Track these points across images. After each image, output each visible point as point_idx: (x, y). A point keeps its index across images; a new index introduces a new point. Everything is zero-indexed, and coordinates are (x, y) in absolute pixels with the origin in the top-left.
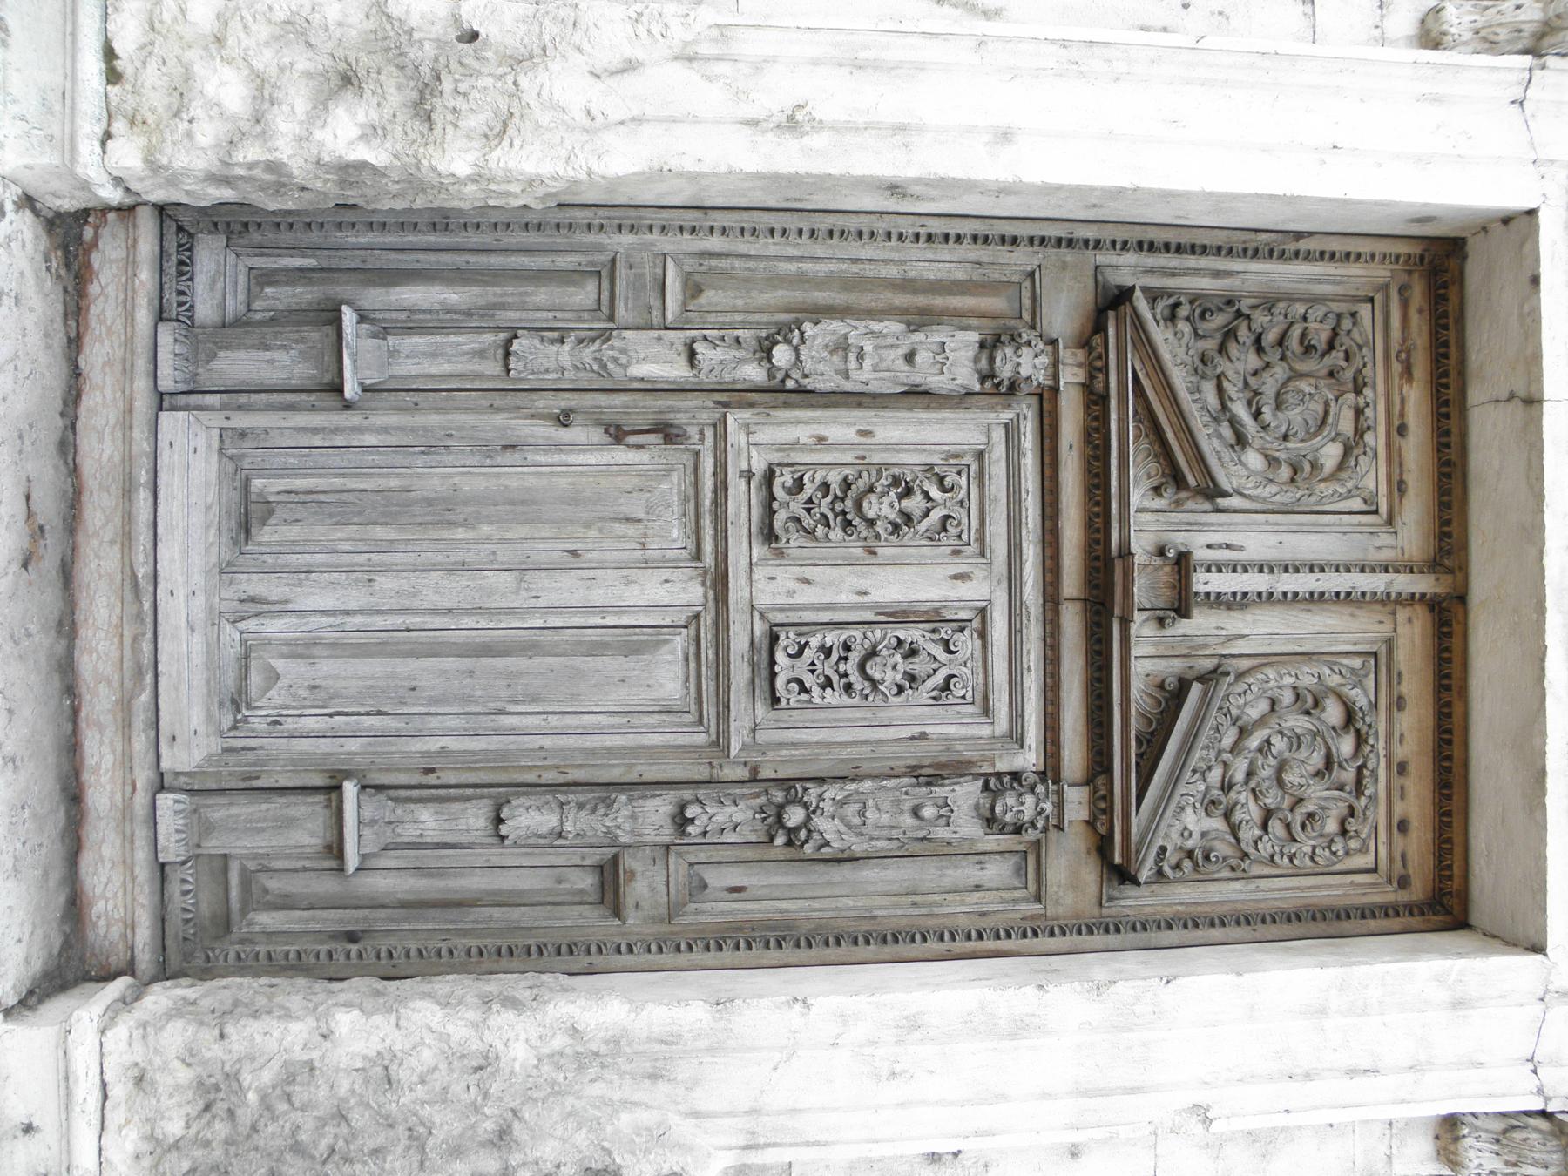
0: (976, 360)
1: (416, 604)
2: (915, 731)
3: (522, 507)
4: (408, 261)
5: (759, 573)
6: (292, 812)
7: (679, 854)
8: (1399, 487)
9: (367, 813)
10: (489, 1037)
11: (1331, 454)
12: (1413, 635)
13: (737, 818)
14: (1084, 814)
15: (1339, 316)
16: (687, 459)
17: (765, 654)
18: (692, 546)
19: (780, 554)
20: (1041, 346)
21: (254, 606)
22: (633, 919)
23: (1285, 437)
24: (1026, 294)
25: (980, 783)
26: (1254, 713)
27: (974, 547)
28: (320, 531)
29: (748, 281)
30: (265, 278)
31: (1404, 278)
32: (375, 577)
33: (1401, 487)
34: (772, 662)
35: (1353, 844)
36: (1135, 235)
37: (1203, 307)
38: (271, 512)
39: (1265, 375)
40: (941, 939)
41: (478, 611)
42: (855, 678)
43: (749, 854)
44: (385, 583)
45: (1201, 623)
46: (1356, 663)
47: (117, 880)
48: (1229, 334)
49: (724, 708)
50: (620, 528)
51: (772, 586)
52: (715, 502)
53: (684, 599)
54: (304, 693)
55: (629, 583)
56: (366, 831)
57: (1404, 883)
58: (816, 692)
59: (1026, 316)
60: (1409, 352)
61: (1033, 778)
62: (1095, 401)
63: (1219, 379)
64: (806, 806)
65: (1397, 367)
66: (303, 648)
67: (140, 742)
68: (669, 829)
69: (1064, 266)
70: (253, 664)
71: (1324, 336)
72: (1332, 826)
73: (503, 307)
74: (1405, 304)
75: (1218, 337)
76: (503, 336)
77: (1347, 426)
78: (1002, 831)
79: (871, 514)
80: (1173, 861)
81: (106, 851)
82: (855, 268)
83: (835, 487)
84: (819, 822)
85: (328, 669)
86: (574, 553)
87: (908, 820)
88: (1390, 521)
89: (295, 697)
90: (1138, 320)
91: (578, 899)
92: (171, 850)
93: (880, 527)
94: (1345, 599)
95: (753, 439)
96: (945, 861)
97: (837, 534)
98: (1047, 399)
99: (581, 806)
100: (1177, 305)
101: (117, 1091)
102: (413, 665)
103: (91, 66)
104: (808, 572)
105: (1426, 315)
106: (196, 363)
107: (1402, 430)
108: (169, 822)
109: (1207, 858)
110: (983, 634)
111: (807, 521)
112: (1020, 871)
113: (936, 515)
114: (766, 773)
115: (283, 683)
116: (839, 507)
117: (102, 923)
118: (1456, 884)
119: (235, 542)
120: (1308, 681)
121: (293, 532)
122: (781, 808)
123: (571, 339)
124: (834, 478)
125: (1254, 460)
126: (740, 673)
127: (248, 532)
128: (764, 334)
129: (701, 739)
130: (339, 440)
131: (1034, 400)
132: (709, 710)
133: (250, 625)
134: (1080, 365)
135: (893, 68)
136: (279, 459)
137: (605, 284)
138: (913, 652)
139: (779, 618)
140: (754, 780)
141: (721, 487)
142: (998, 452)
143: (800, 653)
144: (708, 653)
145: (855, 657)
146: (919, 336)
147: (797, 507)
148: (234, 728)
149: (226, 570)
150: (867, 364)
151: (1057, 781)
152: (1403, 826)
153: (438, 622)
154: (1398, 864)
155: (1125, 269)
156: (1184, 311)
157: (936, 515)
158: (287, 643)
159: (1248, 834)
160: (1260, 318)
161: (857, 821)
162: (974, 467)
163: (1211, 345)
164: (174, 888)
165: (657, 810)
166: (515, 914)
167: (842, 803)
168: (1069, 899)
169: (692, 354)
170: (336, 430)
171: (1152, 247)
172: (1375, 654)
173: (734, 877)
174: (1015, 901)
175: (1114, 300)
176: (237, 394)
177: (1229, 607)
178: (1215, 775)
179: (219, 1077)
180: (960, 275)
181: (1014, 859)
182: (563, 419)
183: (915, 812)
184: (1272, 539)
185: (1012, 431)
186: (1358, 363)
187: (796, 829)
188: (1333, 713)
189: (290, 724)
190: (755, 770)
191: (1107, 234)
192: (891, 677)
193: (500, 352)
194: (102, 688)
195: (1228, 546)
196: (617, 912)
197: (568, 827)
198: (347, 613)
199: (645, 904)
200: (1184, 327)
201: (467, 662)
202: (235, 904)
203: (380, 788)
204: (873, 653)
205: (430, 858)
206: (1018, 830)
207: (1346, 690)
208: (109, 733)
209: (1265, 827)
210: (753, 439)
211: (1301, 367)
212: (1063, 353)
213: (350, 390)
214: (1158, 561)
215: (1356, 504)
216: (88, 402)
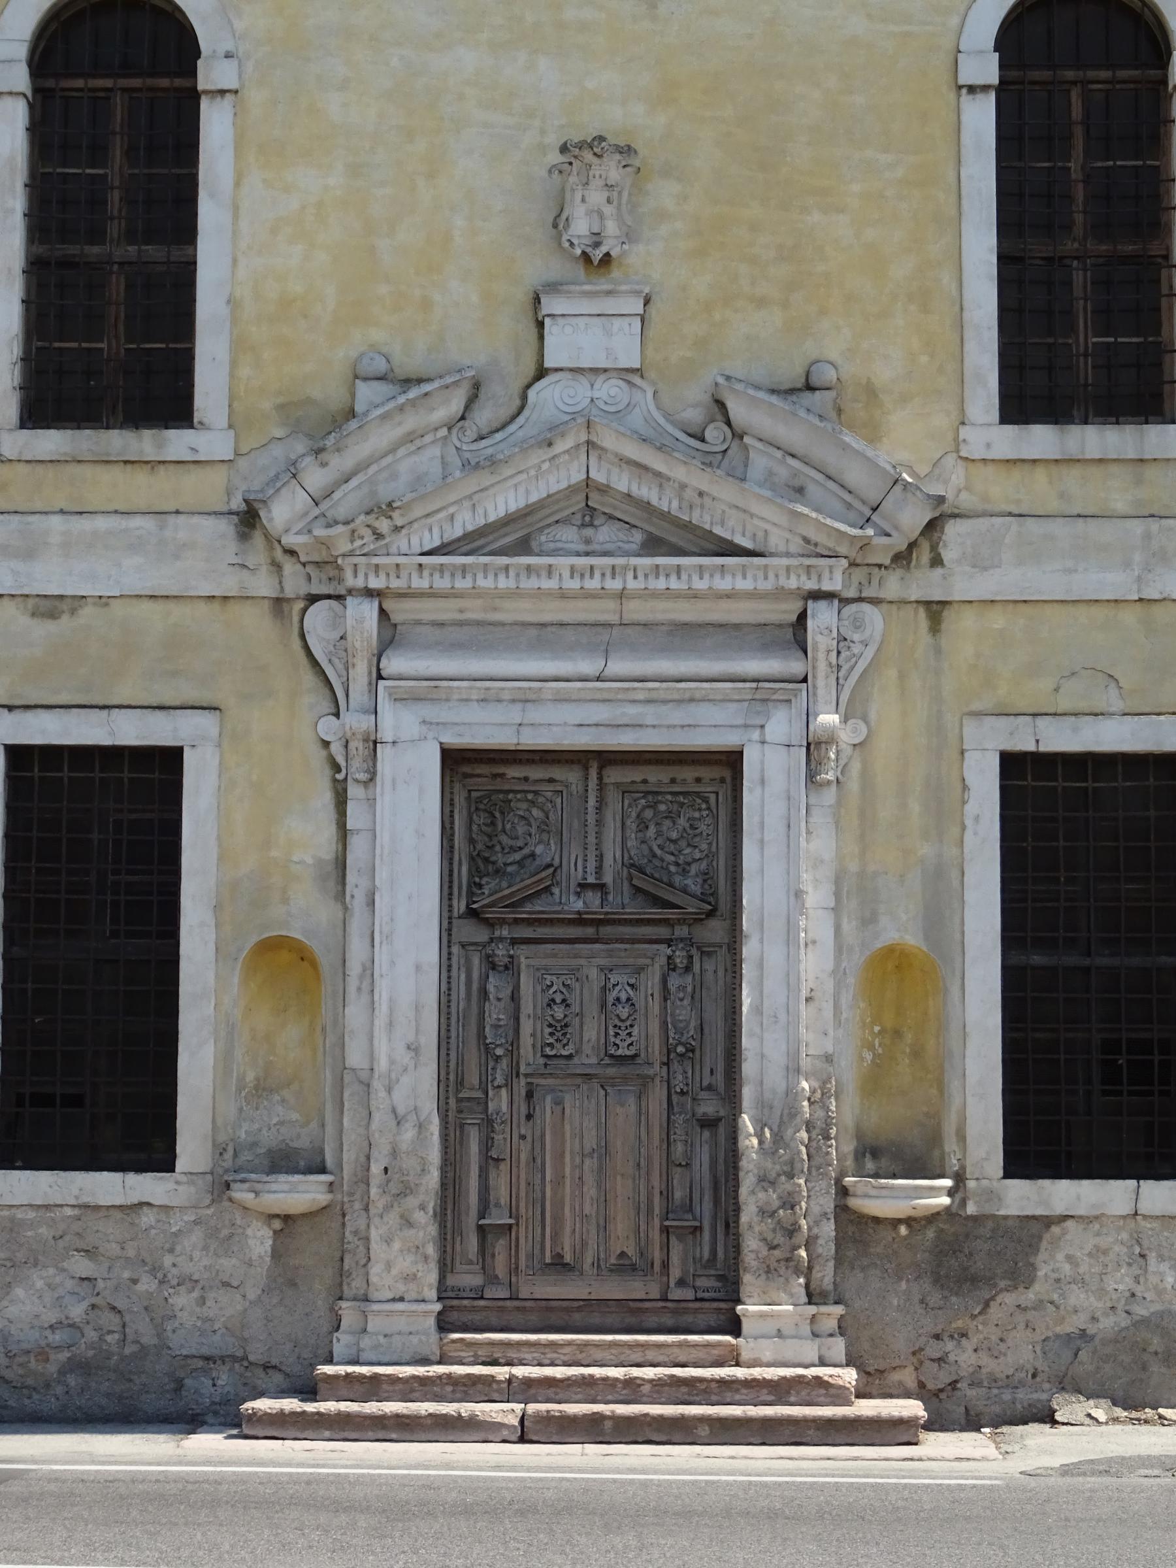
0: (500, 972)
7: (697, 1095)
12: (615, 775)
20: (493, 944)
22: (722, 1113)
23: (530, 835)
32: (532, 1019)
33: (551, 781)
36: (446, 902)
37: (475, 871)
40: (735, 989)
42: (628, 1023)
45: (608, 879)
46: (626, 802)
48: (486, 860)
63: (505, 864)
64: (677, 1045)
67: (647, 1305)
72: (697, 815)
76: (490, 1161)
79: (562, 1016)
83: (550, 1030)
87: (686, 1002)
90: (483, 907)
91: (714, 1135)
94: (599, 809)
97: (569, 1030)
98: (514, 942)
100: (475, 883)
103: (400, 1306)
105: (475, 765)
107: (526, 779)
109: (706, 874)
111: (565, 1041)
112: (709, 954)
114: (665, 1060)
116: (559, 1029)
117: (719, 1322)
118: (723, 758)
120: (634, 826)
125: (539, 850)
134: (501, 928)
135: (391, 1010)
138: (618, 999)
140: (667, 1064)
145: (619, 1024)
146: (491, 997)
147: (558, 1045)
151: (671, 940)
155: (460, 906)
156: (477, 880)
159: (697, 855)
160: (480, 846)
166: (721, 1160)
169: (499, 1087)
171: (451, 894)
173: (707, 1071)
176: (514, 1270)
178: (673, 869)
183: (681, 1000)
188: (649, 814)
190: (664, 1064)
191: (446, 914)
196: (719, 1119)
206: (691, 957)
209: (696, 847)
211: (500, 827)
212: (497, 933)
213: (512, 1221)
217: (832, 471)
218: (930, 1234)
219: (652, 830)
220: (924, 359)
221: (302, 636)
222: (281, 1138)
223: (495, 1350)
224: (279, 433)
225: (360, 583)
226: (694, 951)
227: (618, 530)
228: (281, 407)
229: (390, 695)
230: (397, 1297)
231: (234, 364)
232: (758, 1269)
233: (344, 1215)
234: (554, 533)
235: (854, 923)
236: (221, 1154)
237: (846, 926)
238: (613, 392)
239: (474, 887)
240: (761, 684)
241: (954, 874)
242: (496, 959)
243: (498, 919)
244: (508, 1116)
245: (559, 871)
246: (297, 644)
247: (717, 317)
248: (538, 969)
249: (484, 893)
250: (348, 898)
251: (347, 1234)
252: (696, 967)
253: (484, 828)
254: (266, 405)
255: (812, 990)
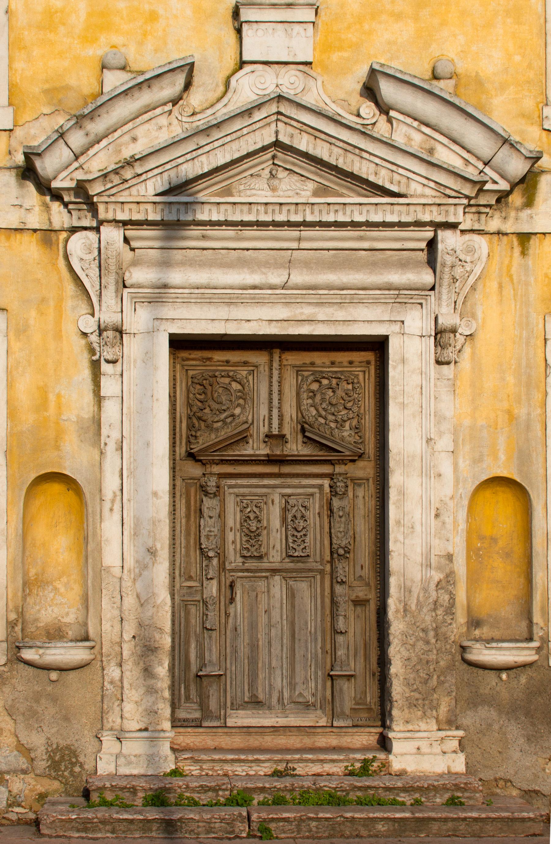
0: (210, 498)
1: (280, 655)
2: (317, 516)
3: (253, 626)
4: (183, 658)
5: (271, 560)
6: (338, 690)
8: (246, 363)
9: (339, 668)
10: (397, 633)
11: (235, 386)
13: (341, 567)
14: (343, 466)
15: (192, 382)
16: (238, 580)
17: (295, 559)
18: (264, 579)
19: (266, 554)
21: (280, 700)
24: (189, 481)
25: (333, 498)
26: (314, 412)
27: (264, 498)
28: (260, 682)
29: (188, 563)
30: (188, 698)
31: (180, 359)
33: (246, 363)
34: (297, 556)
35: (356, 381)
37: (191, 427)
38: (255, 695)
39: (212, 407)
41: (282, 638)
42: (302, 533)
43: (352, 564)
44: (274, 664)
45: (286, 431)
46: (300, 378)
47: (357, 737)
48: (199, 419)
49: (310, 570)
50: (259, 599)
51: (275, 557)
52: (251, 572)
53: (279, 582)
54: (305, 686)
55: (274, 596)
56: (344, 669)
57: (368, 363)
58: (306, 544)
59: (196, 481)
60: (204, 359)
61: (332, 482)
62: (222, 462)
64: (338, 548)
65: (208, 363)
66: (292, 686)
68: (344, 586)
69: (180, 470)
70: (297, 700)
71: (198, 387)
73: (196, 631)
74: (188, 359)
75: (201, 422)
77: (227, 380)
78: (347, 491)
79: (255, 528)
80: (358, 438)
81: (349, 740)
82: (183, 532)
84: (343, 544)
85: (299, 679)
86: (266, 612)
87: (343, 519)
88: (257, 367)
89: (306, 689)
92: (349, 723)
93: (259, 526)
94: (280, 377)
95: (233, 561)
96: (356, 507)
97: (261, 538)
99: (337, 610)
100: (192, 435)
101: (410, 727)
102: (297, 656)
104: (271, 546)
106: (212, 716)
107: (228, 362)
108: (341, 723)
110: (289, 496)
111: (257, 547)
112: (359, 485)
113: (255, 509)
115: (302, 692)
119: (262, 706)
121: (260, 689)
122: (339, 555)
123: (206, 612)
124: (244, 539)
126: (300, 565)
127: (260, 702)
128: (204, 559)
129: (318, 577)
130: (234, 677)
131: (221, 479)
132: (311, 574)
133: (286, 702)
136: (239, 694)
137: (189, 603)
139: (284, 555)
141: (247, 570)
142: (236, 490)
143: (295, 549)
144: (294, 574)
145: (296, 533)
146: (205, 515)
147: (253, 549)
148: (315, 706)
149: (270, 708)
150: (212, 529)
152: (351, 363)
153: (285, 649)
154: (363, 364)
155: (181, 450)
156: (194, 433)
157: (255, 509)
158: (291, 691)
159: (351, 416)
160: (195, 409)
161: (343, 534)
162: (241, 498)
163: (203, 424)
164: (360, 723)
165: (339, 589)
167: (338, 537)
168: (368, 470)
169: (211, 579)
170: (231, 678)
172: (297, 371)
173: (358, 568)
174: (368, 486)
175: (191, 456)
177: (282, 420)
178: (333, 425)
179: (407, 703)
180: (184, 501)
181: (356, 487)
182: (227, 615)
184: (262, 406)
185: (230, 487)
186: (207, 377)
187: (345, 551)
189: (313, 691)
190: (328, 562)
192: (302, 524)
193: (210, 632)
194: (304, 741)
195: (264, 420)
196: (368, 601)
197: (343, 614)
198: (282, 674)
199: (366, 593)
200: (198, 434)
201: (297, 641)
202: (365, 707)
203: (332, 666)
204: (295, 529)
205: (352, 652)
206: (347, 486)
207: (308, 383)
208: (316, 739)
210: (233, 561)
212: (208, 470)
214: (269, 443)
215: (250, 378)
216: (223, 745)
217: (455, 135)
218: (523, 680)
219: (318, 398)
220: (517, 58)
221: (66, 257)
222: (54, 616)
223: (215, 764)
224: (46, 110)
225: (110, 216)
226: (349, 482)
227: (296, 181)
228: (46, 92)
229: (132, 298)
230: (143, 728)
231: (11, 59)
232: (403, 706)
233: (103, 669)
234: (249, 184)
235: (468, 462)
236: (13, 627)
237: (462, 464)
238: (292, 80)
239: (191, 438)
240: (402, 292)
241: (538, 428)
242: (208, 489)
243: (209, 460)
244: (217, 600)
245: (252, 427)
246: (61, 262)
247: (366, 27)
248: (237, 496)
249: (198, 443)
250: (102, 445)
251: (106, 683)
252: (350, 494)
253: (198, 396)
254: (36, 90)
255: (438, 509)
